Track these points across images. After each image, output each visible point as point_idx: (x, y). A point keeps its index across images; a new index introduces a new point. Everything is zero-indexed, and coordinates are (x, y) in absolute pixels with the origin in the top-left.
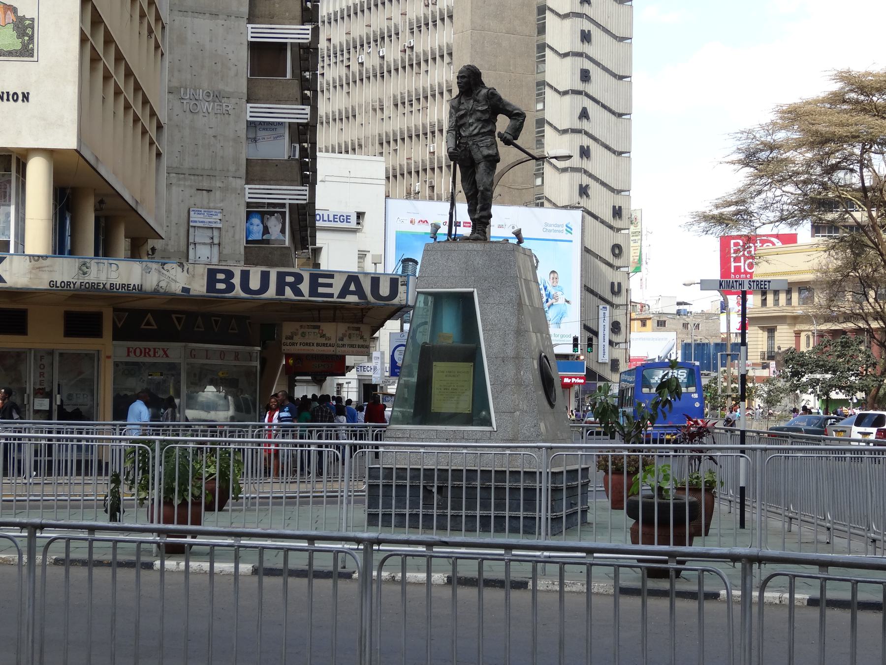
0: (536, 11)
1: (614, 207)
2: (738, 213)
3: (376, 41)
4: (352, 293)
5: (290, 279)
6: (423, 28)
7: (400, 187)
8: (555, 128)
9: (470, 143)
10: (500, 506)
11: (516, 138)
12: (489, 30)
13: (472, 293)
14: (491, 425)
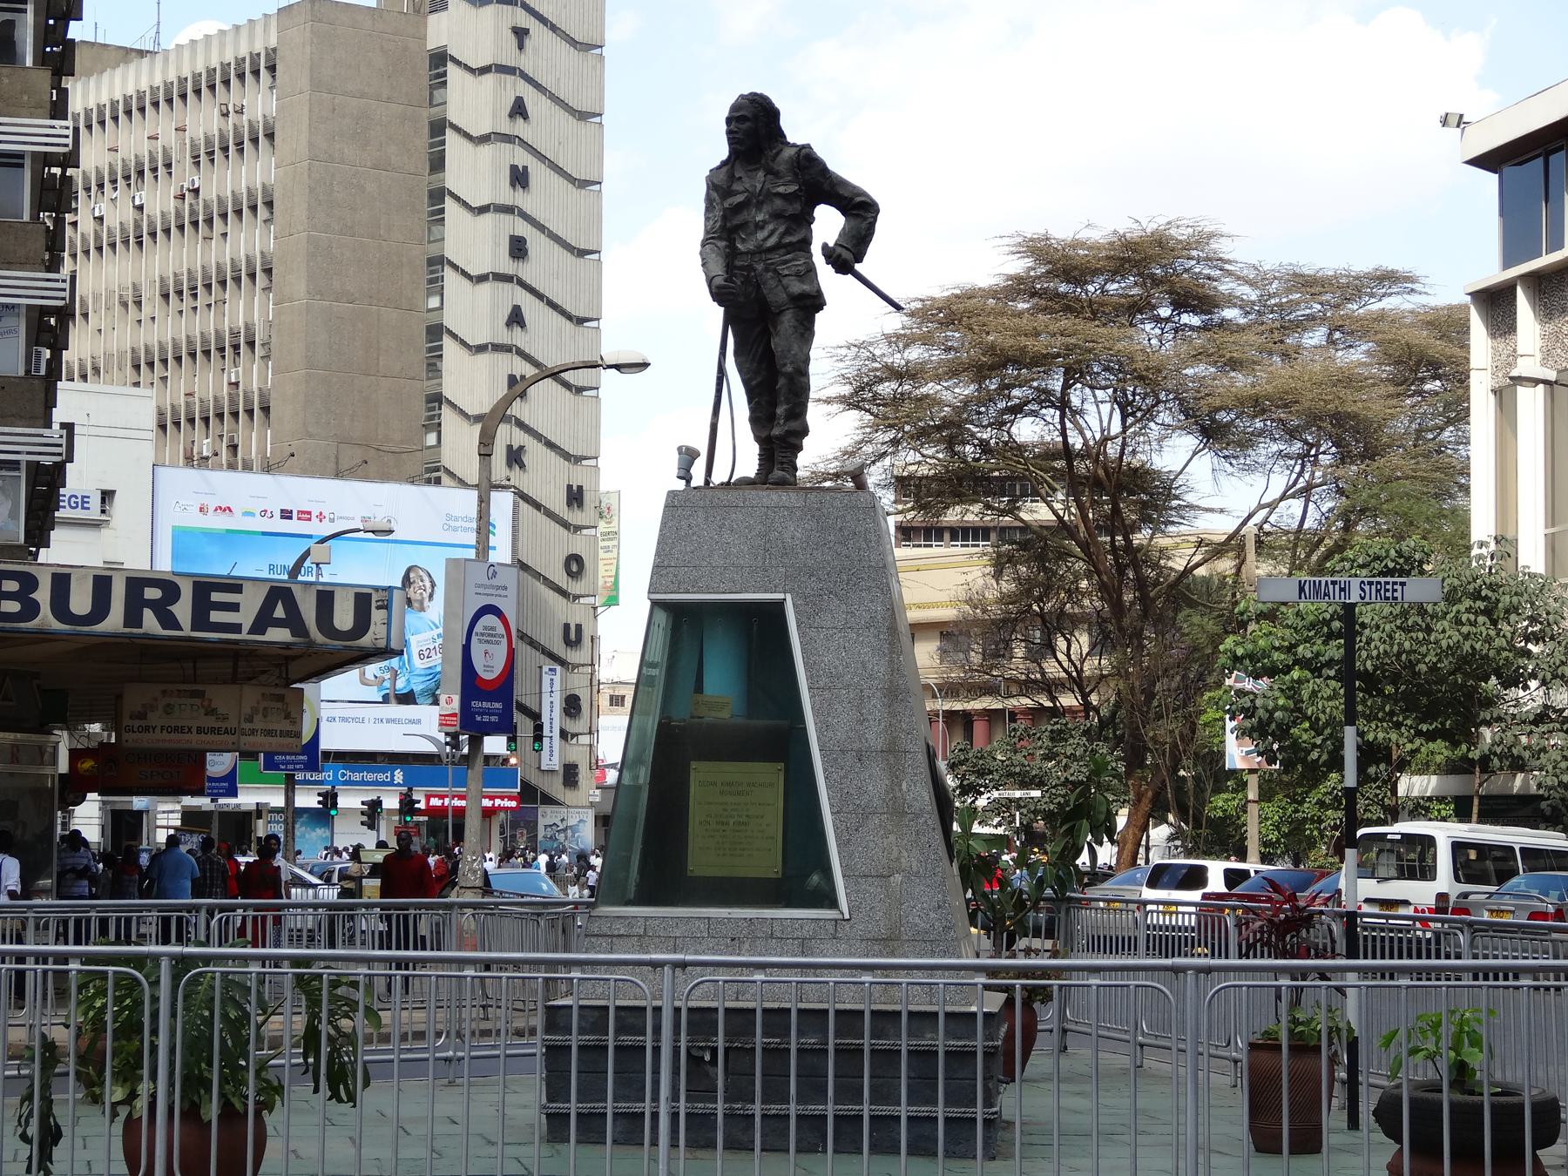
0: (426, 130)
1: (570, 487)
3: (127, 178)
4: (279, 623)
5: (152, 593)
6: (218, 155)
7: (176, 445)
8: (463, 343)
9: (760, 267)
10: (848, 1091)
11: (859, 259)
12: (343, 162)
13: (780, 605)
14: (833, 903)
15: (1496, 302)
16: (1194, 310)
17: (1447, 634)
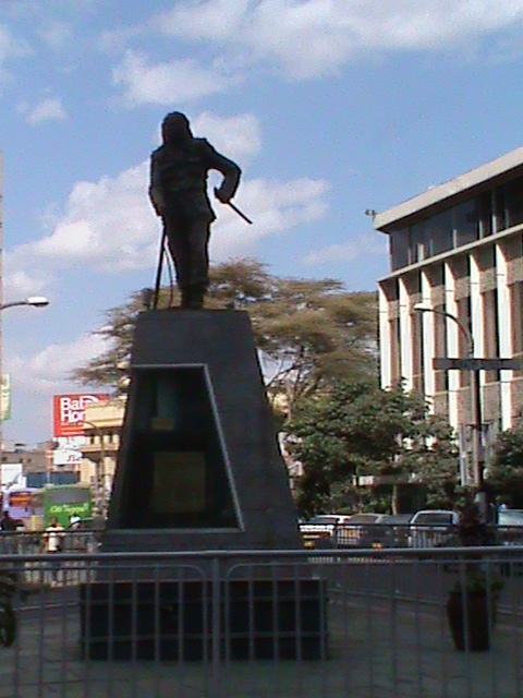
2: (109, 369)
11: (232, 196)
13: (202, 368)
14: (233, 522)
15: (390, 288)
16: (253, 295)
17: (383, 417)
